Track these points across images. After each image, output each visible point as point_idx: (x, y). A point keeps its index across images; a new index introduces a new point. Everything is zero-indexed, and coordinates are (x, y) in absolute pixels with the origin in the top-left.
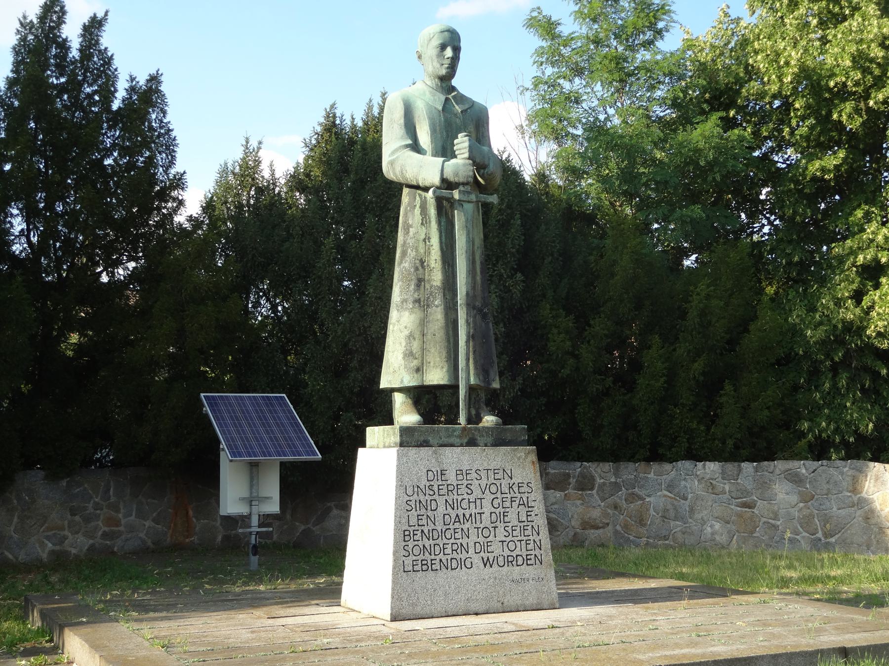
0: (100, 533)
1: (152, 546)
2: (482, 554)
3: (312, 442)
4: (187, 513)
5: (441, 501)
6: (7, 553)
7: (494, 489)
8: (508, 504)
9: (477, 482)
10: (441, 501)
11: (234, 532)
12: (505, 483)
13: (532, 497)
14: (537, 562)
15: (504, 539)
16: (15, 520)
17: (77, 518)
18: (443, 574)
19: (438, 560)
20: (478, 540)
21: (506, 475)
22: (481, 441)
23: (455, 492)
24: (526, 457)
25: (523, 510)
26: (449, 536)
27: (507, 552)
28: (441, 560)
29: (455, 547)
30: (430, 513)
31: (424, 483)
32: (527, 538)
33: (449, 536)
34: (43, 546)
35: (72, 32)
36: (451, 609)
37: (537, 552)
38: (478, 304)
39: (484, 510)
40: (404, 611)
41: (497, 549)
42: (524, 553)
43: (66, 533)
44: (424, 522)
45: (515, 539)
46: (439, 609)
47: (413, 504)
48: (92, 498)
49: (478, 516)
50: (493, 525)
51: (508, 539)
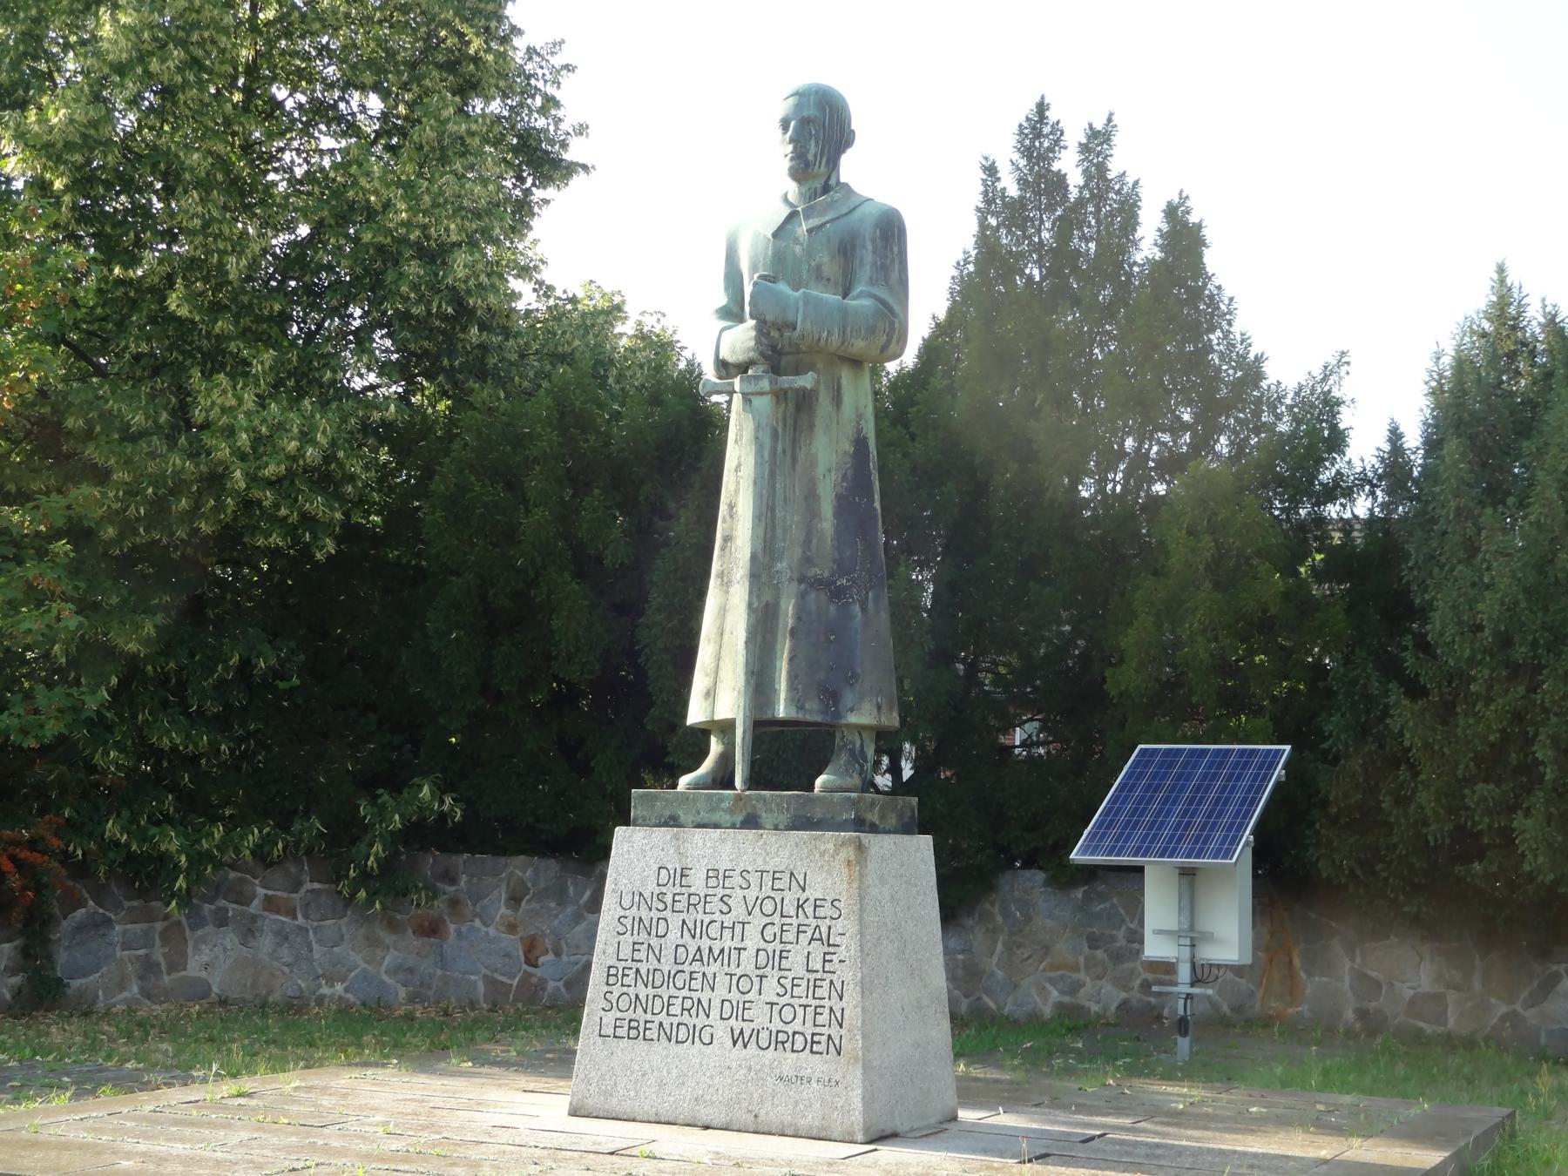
0: (1138, 982)
1: (1228, 1013)
2: (732, 1022)
3: (1086, 832)
4: (1291, 961)
5: (675, 921)
6: (986, 999)
7: (768, 907)
8: (790, 936)
9: (741, 893)
10: (675, 921)
11: (1373, 1004)
12: (790, 898)
13: (838, 926)
14: (832, 1048)
15: (775, 999)
16: (1000, 947)
17: (1100, 954)
18: (659, 1053)
19: (656, 1024)
20: (728, 997)
21: (794, 883)
22: (766, 818)
23: (700, 908)
24: (837, 852)
25: (818, 950)
26: (679, 984)
27: (777, 1024)
28: (661, 1024)
29: (688, 1004)
30: (654, 941)
31: (651, 888)
32: (817, 1002)
33: (679, 984)
34: (1042, 991)
35: (1069, 165)
36: (666, 1111)
37: (834, 1031)
38: (822, 570)
39: (748, 943)
40: (590, 1101)
41: (759, 1016)
42: (809, 1031)
43: (1082, 976)
44: (642, 955)
45: (796, 1002)
46: (646, 1107)
47: (628, 923)
48: (1123, 921)
49: (734, 954)
50: (759, 972)
51: (782, 1001)
